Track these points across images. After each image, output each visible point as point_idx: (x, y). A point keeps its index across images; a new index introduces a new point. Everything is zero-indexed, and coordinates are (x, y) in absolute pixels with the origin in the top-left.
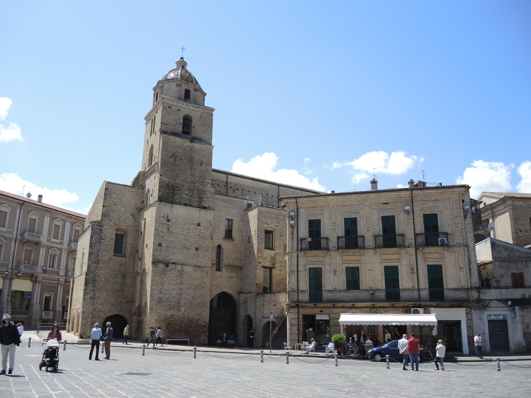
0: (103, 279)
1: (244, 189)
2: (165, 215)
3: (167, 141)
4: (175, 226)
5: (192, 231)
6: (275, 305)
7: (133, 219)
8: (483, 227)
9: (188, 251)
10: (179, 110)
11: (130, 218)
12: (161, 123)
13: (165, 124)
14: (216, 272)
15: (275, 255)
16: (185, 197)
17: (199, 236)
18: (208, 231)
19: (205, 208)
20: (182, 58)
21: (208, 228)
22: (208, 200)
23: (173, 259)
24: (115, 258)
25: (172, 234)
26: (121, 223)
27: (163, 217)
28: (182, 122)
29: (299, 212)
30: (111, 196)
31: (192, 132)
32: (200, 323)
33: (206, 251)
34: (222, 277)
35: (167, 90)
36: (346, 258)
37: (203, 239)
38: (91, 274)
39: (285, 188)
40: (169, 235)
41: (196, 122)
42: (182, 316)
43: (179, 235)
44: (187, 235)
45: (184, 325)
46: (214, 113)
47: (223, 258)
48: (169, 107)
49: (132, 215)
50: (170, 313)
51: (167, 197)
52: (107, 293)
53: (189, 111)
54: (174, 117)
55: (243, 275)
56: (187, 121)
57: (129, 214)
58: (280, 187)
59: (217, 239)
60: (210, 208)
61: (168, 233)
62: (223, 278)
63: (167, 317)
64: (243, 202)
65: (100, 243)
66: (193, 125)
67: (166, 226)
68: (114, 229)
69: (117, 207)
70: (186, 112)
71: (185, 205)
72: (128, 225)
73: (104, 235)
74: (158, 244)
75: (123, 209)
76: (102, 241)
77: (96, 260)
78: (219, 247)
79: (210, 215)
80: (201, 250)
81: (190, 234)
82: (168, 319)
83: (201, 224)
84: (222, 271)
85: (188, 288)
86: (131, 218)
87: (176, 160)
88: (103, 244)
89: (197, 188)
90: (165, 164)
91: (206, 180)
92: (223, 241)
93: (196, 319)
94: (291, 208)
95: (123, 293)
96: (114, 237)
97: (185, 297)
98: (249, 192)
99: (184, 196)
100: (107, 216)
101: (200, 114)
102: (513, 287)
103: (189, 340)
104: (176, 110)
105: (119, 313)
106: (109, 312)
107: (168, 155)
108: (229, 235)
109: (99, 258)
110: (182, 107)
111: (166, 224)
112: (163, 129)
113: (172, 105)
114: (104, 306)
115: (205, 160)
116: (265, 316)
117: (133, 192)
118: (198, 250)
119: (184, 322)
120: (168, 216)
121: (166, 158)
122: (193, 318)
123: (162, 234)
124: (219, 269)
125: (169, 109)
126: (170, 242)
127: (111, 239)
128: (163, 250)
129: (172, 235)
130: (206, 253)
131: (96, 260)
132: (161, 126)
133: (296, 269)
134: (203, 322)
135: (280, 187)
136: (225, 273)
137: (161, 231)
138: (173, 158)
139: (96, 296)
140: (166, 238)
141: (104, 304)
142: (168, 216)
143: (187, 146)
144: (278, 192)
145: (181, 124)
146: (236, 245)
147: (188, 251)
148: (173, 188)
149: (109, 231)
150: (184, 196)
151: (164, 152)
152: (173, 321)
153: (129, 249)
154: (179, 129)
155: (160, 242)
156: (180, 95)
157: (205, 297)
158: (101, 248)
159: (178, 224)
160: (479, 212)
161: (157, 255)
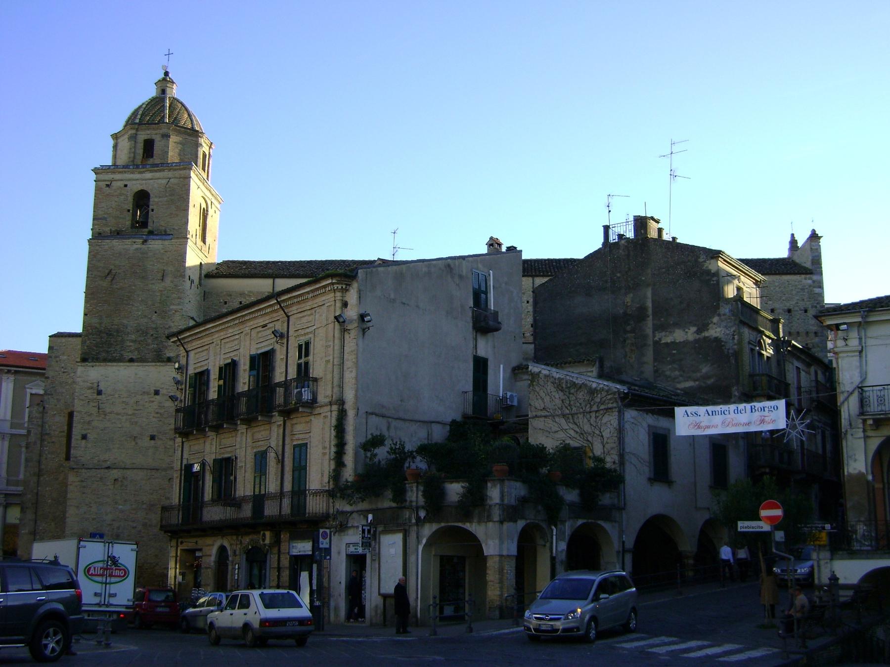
5: (144, 406)
8: (722, 317)
9: (137, 443)
10: (126, 186)
13: (101, 219)
16: (130, 346)
17: (157, 413)
25: (105, 415)
30: (58, 359)
36: (224, 441)
40: (101, 418)
41: (156, 200)
43: (120, 417)
44: (134, 414)
51: (98, 352)
56: (142, 199)
66: (151, 207)
69: (68, 376)
70: (136, 187)
73: (49, 426)
74: (81, 436)
80: (161, 439)
81: (140, 412)
88: (49, 443)
89: (154, 326)
90: (92, 294)
99: (128, 344)
100: (52, 395)
103: (304, 612)
107: (99, 276)
110: (130, 180)
111: (95, 399)
118: (154, 439)
123: (88, 419)
125: (107, 188)
126: (102, 430)
128: (89, 445)
137: (86, 413)
138: (109, 278)
140: (95, 423)
142: (98, 386)
143: (137, 249)
148: (107, 334)
149: (57, 418)
150: (128, 344)
155: (84, 432)
158: (45, 448)
160: (715, 279)
161: (78, 455)
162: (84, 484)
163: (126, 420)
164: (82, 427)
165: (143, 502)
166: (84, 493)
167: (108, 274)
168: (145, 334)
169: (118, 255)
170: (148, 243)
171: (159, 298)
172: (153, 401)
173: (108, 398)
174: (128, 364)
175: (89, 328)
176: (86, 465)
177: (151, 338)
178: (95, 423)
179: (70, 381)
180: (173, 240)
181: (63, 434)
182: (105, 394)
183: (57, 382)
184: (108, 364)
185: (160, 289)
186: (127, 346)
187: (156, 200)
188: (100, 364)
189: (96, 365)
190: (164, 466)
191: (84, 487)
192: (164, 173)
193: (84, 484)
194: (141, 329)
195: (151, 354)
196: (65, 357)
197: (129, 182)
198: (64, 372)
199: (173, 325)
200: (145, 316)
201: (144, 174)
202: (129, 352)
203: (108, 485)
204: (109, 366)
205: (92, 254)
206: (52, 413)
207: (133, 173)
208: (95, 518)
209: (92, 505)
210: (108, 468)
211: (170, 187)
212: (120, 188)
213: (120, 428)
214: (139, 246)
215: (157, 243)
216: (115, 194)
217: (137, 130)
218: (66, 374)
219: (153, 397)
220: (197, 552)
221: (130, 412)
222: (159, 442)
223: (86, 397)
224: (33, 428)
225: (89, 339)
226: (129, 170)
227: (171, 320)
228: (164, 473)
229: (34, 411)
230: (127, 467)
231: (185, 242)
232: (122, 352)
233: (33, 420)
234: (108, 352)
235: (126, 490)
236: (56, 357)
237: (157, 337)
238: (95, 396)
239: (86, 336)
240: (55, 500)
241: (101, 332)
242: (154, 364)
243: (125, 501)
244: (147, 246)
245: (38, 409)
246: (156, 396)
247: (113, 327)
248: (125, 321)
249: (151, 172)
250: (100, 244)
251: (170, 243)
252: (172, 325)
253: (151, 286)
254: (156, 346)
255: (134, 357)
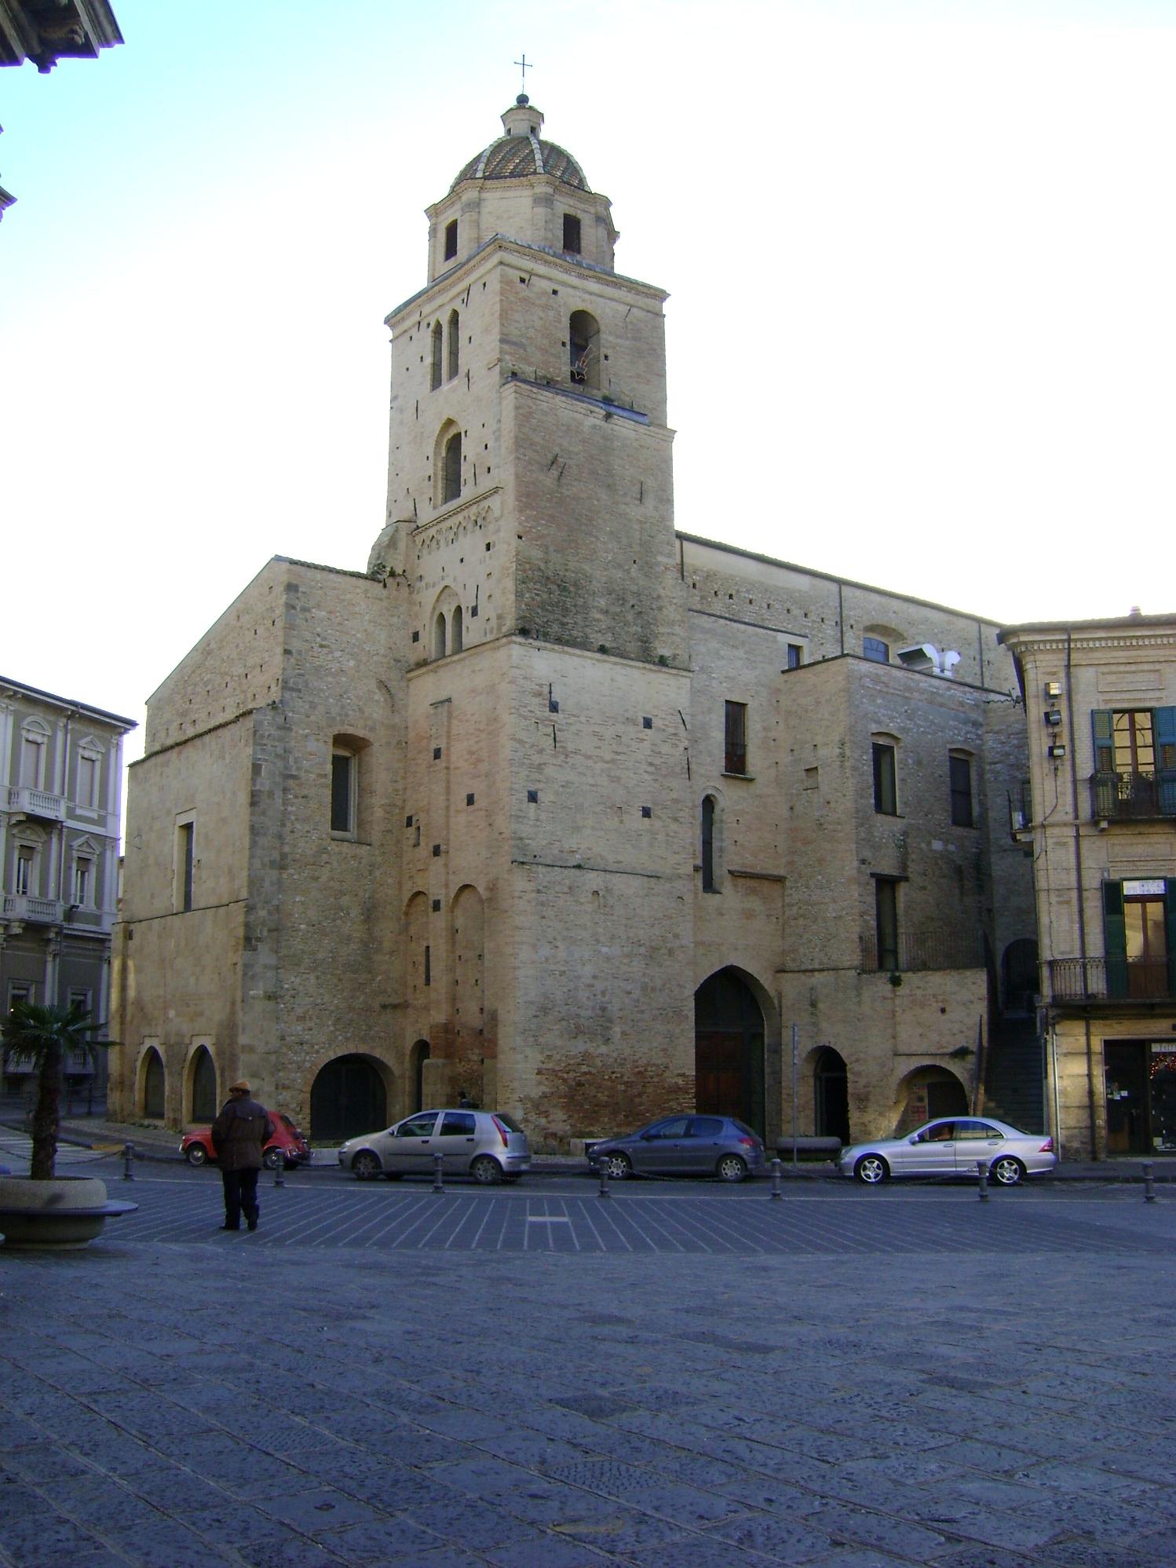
0: (302, 926)
1: (734, 593)
2: (541, 685)
3: (530, 408)
4: (573, 728)
6: (943, 1011)
7: (385, 700)
9: (621, 822)
10: (555, 292)
11: (376, 697)
12: (502, 341)
13: (514, 344)
14: (706, 895)
15: (905, 834)
16: (599, 620)
17: (651, 764)
18: (677, 746)
19: (662, 662)
20: (523, 100)
21: (675, 734)
22: (669, 631)
23: (575, 847)
24: (333, 847)
25: (567, 756)
26: (347, 715)
27: (540, 694)
28: (567, 339)
29: (1072, 680)
30: (308, 615)
31: (603, 376)
32: (672, 1079)
33: (676, 820)
34: (722, 915)
35: (498, 218)
37: (665, 776)
38: (263, 908)
39: (858, 593)
41: (611, 338)
42: (615, 1055)
43: (590, 763)
44: (613, 761)
45: (623, 1087)
46: (667, 307)
47: (725, 844)
48: (522, 280)
49: (383, 686)
50: (580, 1046)
52: (317, 978)
53: (587, 296)
54: (541, 319)
55: (791, 905)
56: (581, 325)
57: (373, 685)
58: (843, 588)
59: (702, 776)
60: (677, 663)
61: (555, 756)
62: (726, 917)
63: (572, 1062)
64: (775, 641)
65: (285, 790)
66: (603, 351)
67: (546, 726)
68: (325, 738)
69: (330, 657)
70: (576, 302)
71: (602, 650)
72: (369, 723)
73: (296, 760)
75: (352, 663)
76: (291, 782)
77: (276, 855)
78: (709, 803)
79: (679, 688)
82: (573, 1068)
83: (656, 722)
84: (723, 890)
85: (628, 956)
86: (378, 696)
87: (563, 481)
88: (296, 797)
89: (635, 588)
90: (528, 495)
91: (660, 558)
92: (721, 784)
93: (657, 1066)
94: (1044, 664)
95: (370, 976)
96: (329, 768)
97: (619, 987)
98: (751, 602)
101: (623, 309)
102: (50, 927)
104: (544, 293)
105: (363, 1049)
106: (330, 1045)
107: (539, 463)
108: (736, 763)
109: (286, 849)
110: (564, 284)
112: (510, 362)
113: (531, 274)
114: (312, 1024)
115: (650, 483)
116: (902, 1049)
117: (381, 600)
119: (622, 1077)
120: (550, 693)
121: (530, 471)
122: (648, 1065)
123: (536, 759)
124: (709, 886)
125: (523, 286)
126: (563, 786)
127: (319, 775)
128: (543, 816)
129: (567, 763)
130: (674, 826)
131: (276, 855)
132: (502, 352)
133: (1074, 884)
134: (679, 1075)
135: (843, 587)
136: (730, 896)
137: (532, 746)
139: (282, 988)
141: (311, 1019)
143: (594, 426)
144: (837, 604)
145: (564, 344)
146: (760, 796)
147: (621, 822)
148: (559, 586)
149: (312, 746)
151: (522, 450)
152: (590, 1073)
153: (379, 813)
154: (562, 367)
155: (532, 789)
156: (550, 235)
157: (679, 985)
159: (583, 719)
161: (523, 835)
162: (542, 898)
163: (602, 770)
164: (528, 776)
165: (639, 941)
166: (544, 917)
167: (553, 463)
168: (621, 602)
169: (565, 428)
170: (613, 421)
171: (637, 535)
172: (643, 740)
173: (569, 721)
174: (598, 656)
175: (527, 566)
176: (721, 856)
177: (632, 612)
178: (549, 771)
179: (334, 667)
180: (651, 428)
181: (323, 780)
182: (563, 711)
183: (308, 665)
184: (566, 648)
185: (638, 517)
186: (595, 620)
187: (611, 338)
188: (553, 647)
189: (545, 649)
190: (667, 871)
191: (542, 904)
192: (619, 291)
193: (542, 898)
194: (614, 590)
195: (633, 643)
196: (323, 613)
197: (562, 288)
198: (322, 646)
199: (663, 595)
200: (620, 566)
201: (585, 282)
202: (596, 631)
203: (582, 904)
204: (567, 653)
205: (521, 411)
206: (301, 732)
207: (567, 271)
208: (564, 972)
209: (558, 944)
210: (579, 867)
211: (631, 323)
212: (546, 293)
213: (593, 785)
214: (598, 422)
215: (626, 425)
216: (538, 302)
217: (556, 189)
218: (325, 650)
219: (641, 732)
220: (1153, 1045)
221: (608, 757)
222: (658, 824)
223: (531, 711)
224: (266, 760)
225: (529, 590)
226: (565, 263)
227: (661, 582)
228: (668, 886)
229: (266, 723)
230: (608, 868)
231: (669, 437)
232: (588, 630)
233: (265, 742)
234: (563, 624)
235: (612, 915)
236: (305, 610)
237: (641, 613)
238: (547, 713)
239: (524, 583)
240: (314, 926)
241: (548, 578)
242: (641, 665)
243: (613, 937)
244: (610, 426)
245: (274, 719)
246: (646, 730)
247: (567, 574)
248: (587, 567)
249: (598, 283)
250: (534, 396)
251: (648, 432)
252: (662, 592)
253: (624, 507)
254: (639, 629)
255: (607, 645)
